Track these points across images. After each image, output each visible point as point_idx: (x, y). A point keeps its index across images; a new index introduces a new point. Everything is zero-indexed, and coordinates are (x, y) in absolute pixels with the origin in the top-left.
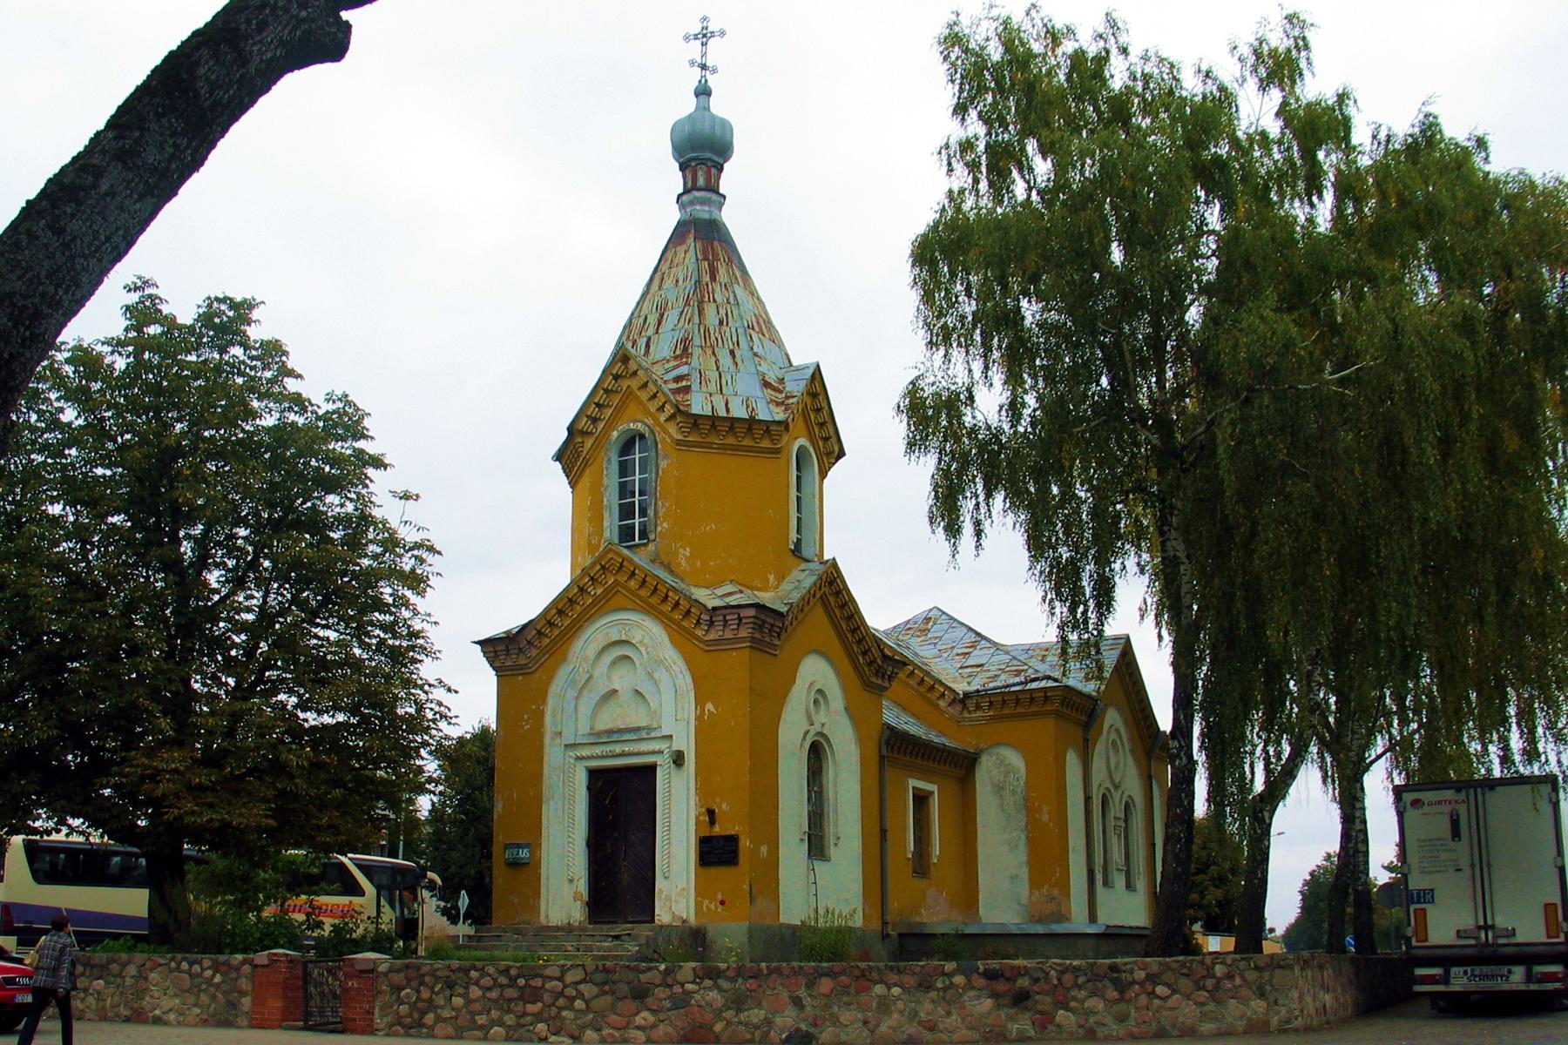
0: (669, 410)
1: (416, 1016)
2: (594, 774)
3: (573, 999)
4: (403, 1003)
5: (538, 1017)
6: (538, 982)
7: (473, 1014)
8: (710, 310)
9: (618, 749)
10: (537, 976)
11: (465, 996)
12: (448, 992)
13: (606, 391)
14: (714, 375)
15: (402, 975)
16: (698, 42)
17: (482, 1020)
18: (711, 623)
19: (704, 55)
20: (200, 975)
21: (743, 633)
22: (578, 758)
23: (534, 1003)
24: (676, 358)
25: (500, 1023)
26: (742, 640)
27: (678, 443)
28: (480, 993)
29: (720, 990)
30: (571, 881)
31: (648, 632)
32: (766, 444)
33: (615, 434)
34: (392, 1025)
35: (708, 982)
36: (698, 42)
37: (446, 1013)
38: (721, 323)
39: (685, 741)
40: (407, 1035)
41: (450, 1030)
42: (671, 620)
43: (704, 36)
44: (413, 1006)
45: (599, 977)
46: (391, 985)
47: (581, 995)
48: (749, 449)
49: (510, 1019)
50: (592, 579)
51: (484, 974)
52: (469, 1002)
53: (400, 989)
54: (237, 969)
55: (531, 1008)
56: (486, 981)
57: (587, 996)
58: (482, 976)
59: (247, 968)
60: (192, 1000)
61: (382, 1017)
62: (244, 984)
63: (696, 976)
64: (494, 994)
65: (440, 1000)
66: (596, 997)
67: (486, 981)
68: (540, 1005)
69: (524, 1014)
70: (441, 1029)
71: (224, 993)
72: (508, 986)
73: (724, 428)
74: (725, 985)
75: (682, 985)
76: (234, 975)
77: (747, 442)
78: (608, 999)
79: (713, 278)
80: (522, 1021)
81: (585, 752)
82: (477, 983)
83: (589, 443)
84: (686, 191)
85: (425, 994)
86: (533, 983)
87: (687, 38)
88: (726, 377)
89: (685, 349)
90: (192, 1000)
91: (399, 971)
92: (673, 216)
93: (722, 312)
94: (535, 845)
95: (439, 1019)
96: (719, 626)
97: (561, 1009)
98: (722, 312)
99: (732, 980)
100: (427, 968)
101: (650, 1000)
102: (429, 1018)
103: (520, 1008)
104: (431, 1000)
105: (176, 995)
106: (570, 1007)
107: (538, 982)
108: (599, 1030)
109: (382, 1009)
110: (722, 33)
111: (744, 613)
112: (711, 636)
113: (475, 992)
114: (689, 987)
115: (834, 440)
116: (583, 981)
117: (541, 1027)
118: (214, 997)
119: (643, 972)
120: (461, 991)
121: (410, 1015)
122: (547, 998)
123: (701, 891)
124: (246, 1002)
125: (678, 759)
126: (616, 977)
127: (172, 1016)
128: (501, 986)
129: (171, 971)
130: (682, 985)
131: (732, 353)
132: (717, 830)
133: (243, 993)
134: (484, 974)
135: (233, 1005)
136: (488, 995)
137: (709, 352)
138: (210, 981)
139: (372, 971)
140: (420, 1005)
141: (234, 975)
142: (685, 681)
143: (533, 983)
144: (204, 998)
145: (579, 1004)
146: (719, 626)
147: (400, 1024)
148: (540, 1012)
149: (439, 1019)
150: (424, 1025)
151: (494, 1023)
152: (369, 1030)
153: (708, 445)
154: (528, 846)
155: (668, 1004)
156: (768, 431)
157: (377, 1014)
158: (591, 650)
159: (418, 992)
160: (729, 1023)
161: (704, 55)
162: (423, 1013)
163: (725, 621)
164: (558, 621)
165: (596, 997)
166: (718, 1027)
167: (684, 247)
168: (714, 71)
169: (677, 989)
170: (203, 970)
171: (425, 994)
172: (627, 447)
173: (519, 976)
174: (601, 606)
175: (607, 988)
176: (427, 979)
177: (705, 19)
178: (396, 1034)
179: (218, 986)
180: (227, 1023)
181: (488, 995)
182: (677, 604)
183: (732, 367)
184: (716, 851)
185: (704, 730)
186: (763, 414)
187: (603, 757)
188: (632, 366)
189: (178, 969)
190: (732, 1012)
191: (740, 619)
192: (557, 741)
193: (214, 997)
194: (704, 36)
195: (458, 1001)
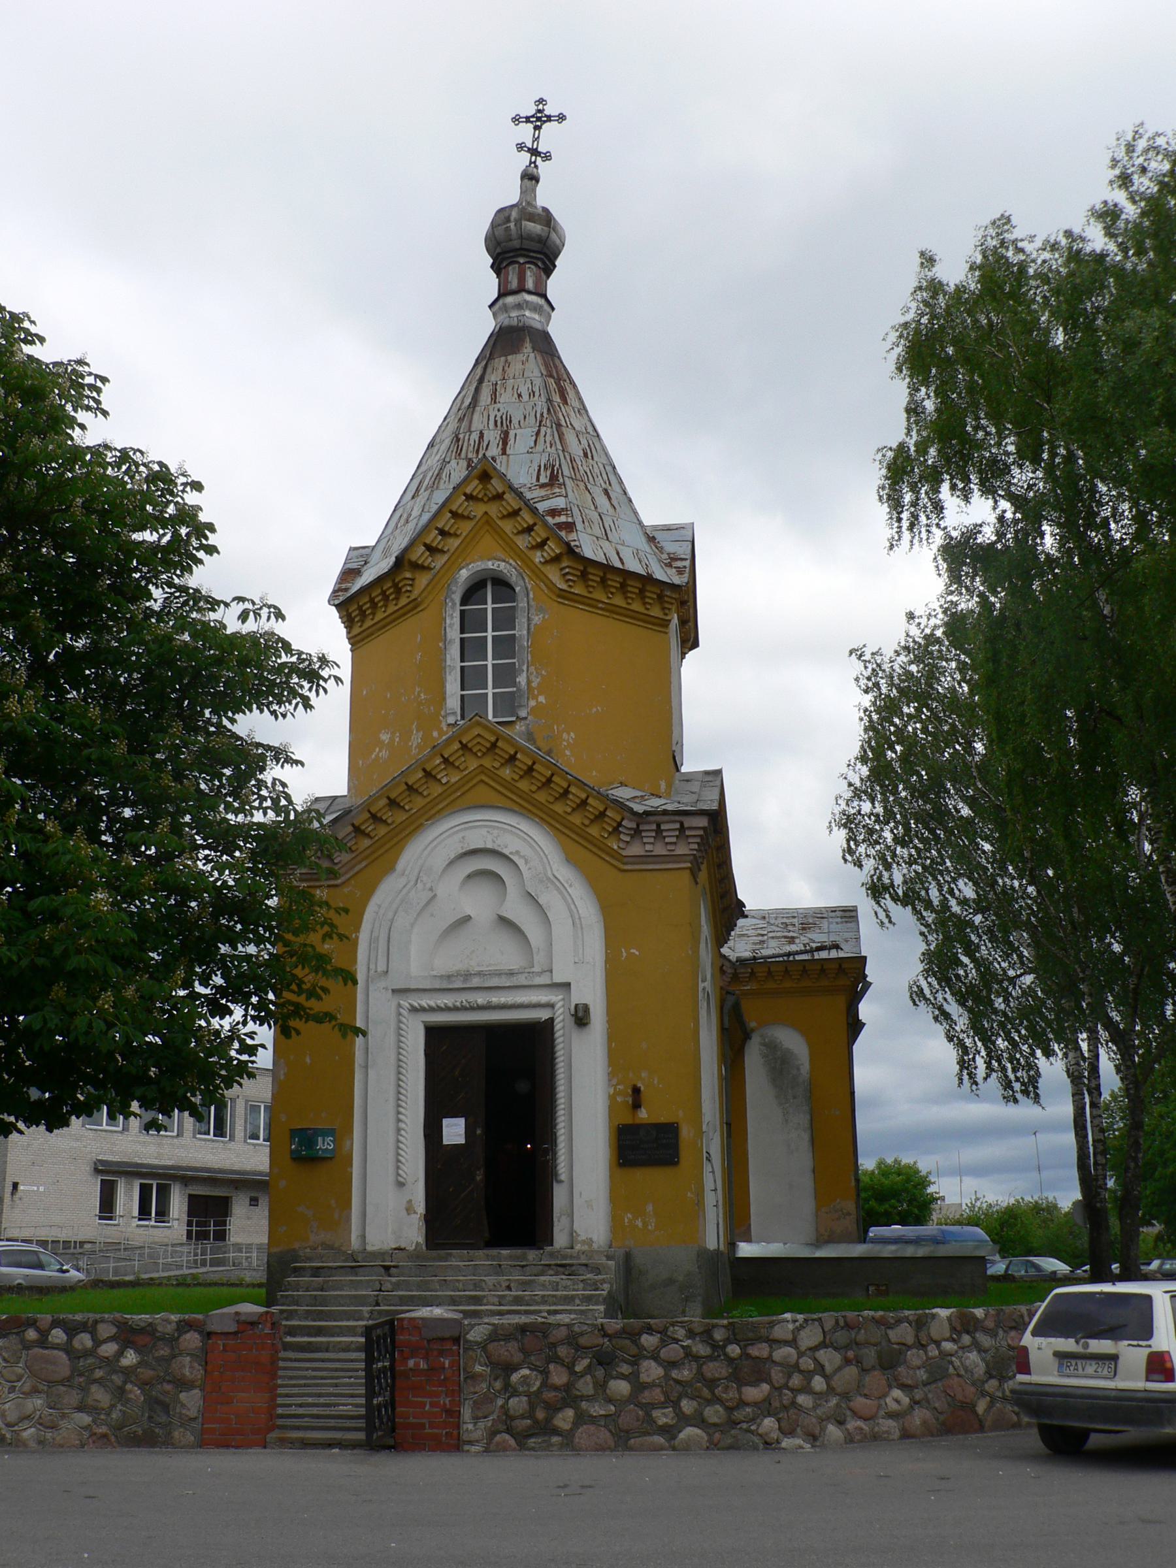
0: (553, 548)
1: (540, 1415)
2: (434, 1034)
3: (808, 1375)
4: (515, 1393)
5: (765, 1408)
6: (759, 1350)
7: (649, 1407)
8: (570, 437)
9: (481, 999)
10: (760, 1339)
11: (632, 1378)
12: (600, 1373)
13: (455, 515)
14: (595, 516)
15: (513, 1346)
16: (531, 126)
17: (663, 1417)
18: (637, 833)
19: (536, 139)
20: (87, 1353)
21: (682, 849)
22: (414, 1010)
23: (755, 1383)
24: (542, 486)
25: (699, 1421)
26: (680, 858)
27: (562, 594)
28: (660, 1371)
29: (981, 1350)
30: (401, 1185)
31: (527, 841)
32: (656, 612)
33: (464, 573)
34: (493, 1433)
35: (966, 1339)
36: (531, 126)
37: (597, 1410)
38: (586, 455)
39: (590, 990)
40: (522, 1446)
41: (604, 1435)
42: (571, 827)
43: (539, 119)
44: (534, 1399)
45: (841, 1337)
46: (492, 1364)
47: (820, 1369)
48: (634, 616)
49: (714, 1413)
50: (446, 761)
51: (667, 1339)
52: (640, 1388)
53: (509, 1368)
54: (172, 1341)
55: (754, 1393)
56: (672, 1351)
57: (829, 1369)
58: (664, 1343)
59: (192, 1339)
60: (74, 1398)
61: (476, 1419)
62: (188, 1368)
63: (953, 1329)
64: (685, 1374)
65: (585, 1386)
66: (839, 1369)
67: (672, 1351)
68: (765, 1387)
69: (742, 1403)
70: (583, 1435)
71: (144, 1384)
72: (710, 1358)
73: (614, 581)
74: (985, 1340)
75: (938, 1343)
76: (164, 1351)
77: (637, 606)
78: (852, 1370)
79: (565, 402)
80: (738, 1415)
81: (426, 1001)
82: (655, 1357)
83: (423, 580)
84: (501, 295)
85: (559, 1377)
86: (754, 1351)
87: (516, 120)
88: (608, 522)
89: (554, 478)
90: (74, 1398)
91: (508, 1338)
92: (486, 325)
93: (584, 442)
94: (342, 1130)
95: (582, 1418)
96: (649, 837)
97: (795, 1391)
98: (584, 442)
99: (993, 1334)
100: (562, 1333)
101: (901, 1369)
102: (565, 1419)
103: (732, 1394)
104: (568, 1387)
105: (35, 1391)
106: (807, 1389)
107: (759, 1350)
108: (841, 1423)
109: (476, 1405)
110: (561, 118)
111: (689, 822)
112: (636, 849)
113: (651, 1371)
114: (948, 1346)
115: (691, 624)
116: (823, 1345)
117: (769, 1423)
118: (120, 1393)
119: (890, 1327)
120: (625, 1369)
121: (531, 1415)
122: (777, 1375)
123: (618, 1200)
124: (191, 1401)
125: (581, 1018)
126: (861, 1337)
127: (29, 1433)
128: (696, 1358)
129: (27, 1345)
130: (938, 1343)
131: (606, 492)
132: (643, 1115)
133: (184, 1384)
134: (667, 1339)
135: (159, 1405)
136: (675, 1374)
137: (582, 485)
138: (110, 1363)
139: (456, 1340)
140: (549, 1395)
141: (164, 1351)
142: (588, 909)
143: (754, 1351)
144: (100, 1396)
145: (818, 1383)
146: (649, 837)
147: (509, 1431)
148: (767, 1400)
149: (582, 1418)
150: (556, 1431)
151: (684, 1420)
152: (454, 1444)
153: (592, 603)
154: (331, 1132)
155: (922, 1375)
156: (660, 597)
157: (467, 1413)
158: (440, 859)
159: (545, 1373)
160: (993, 1400)
161: (536, 139)
162: (554, 1409)
163: (659, 831)
164: (387, 815)
165: (839, 1369)
166: (981, 1407)
167: (520, 357)
168: (547, 157)
169: (933, 1351)
170: (98, 1343)
171: (559, 1377)
172: (473, 592)
173: (728, 1341)
174: (454, 801)
175: (851, 1354)
176: (562, 1351)
177: (541, 101)
178: (503, 1448)
179: (128, 1372)
180: (147, 1440)
181: (675, 1374)
182: (584, 803)
183: (611, 510)
184: (643, 1145)
185: (617, 974)
186: (659, 574)
187: (455, 1009)
188: (497, 485)
189: (43, 1342)
190: (993, 1383)
191: (682, 829)
192: (382, 984)
193: (120, 1393)
194: (539, 119)
195: (621, 1387)
